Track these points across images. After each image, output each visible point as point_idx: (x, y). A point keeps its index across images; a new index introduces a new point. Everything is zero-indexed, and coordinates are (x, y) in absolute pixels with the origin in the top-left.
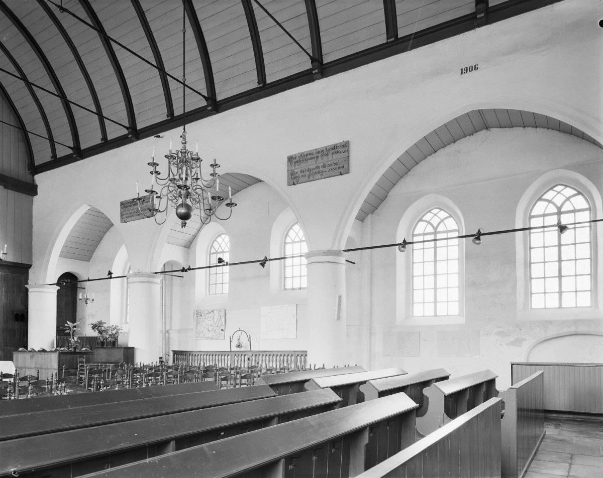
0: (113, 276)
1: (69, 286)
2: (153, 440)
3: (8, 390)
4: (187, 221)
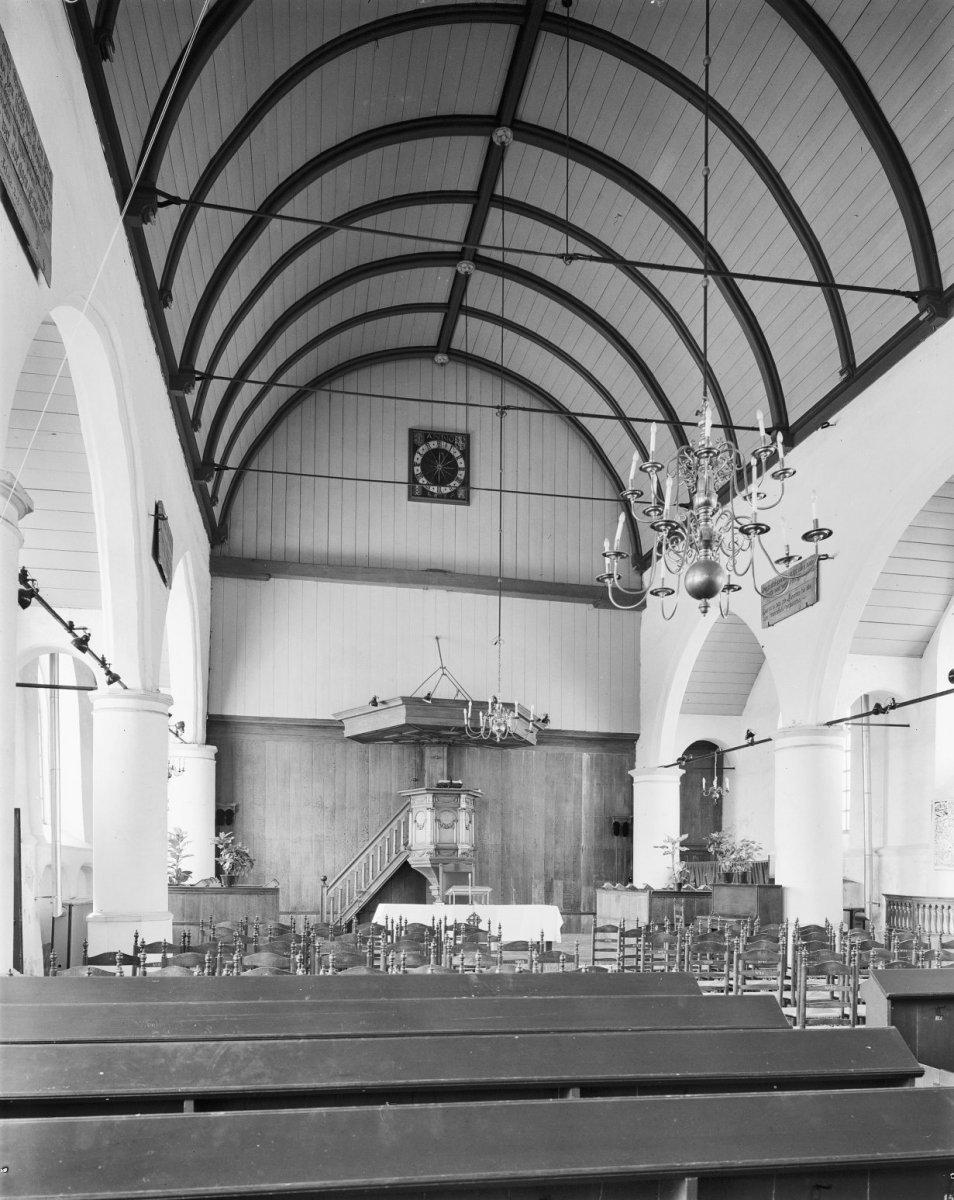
0: (756, 739)
1: (704, 761)
2: (133, 1090)
3: (402, 956)
4: (709, 601)
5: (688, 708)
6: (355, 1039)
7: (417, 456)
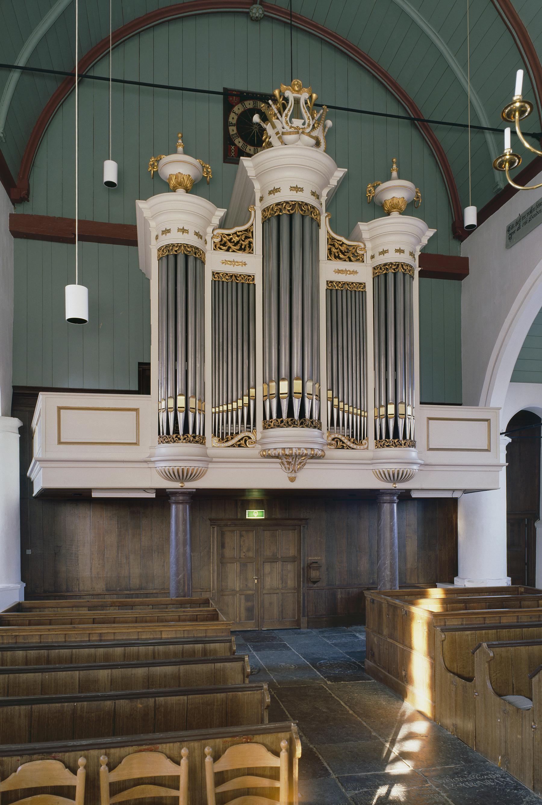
5: (519, 376)
6: (128, 638)
7: (232, 115)
